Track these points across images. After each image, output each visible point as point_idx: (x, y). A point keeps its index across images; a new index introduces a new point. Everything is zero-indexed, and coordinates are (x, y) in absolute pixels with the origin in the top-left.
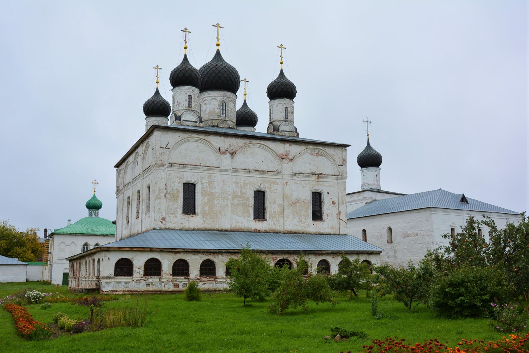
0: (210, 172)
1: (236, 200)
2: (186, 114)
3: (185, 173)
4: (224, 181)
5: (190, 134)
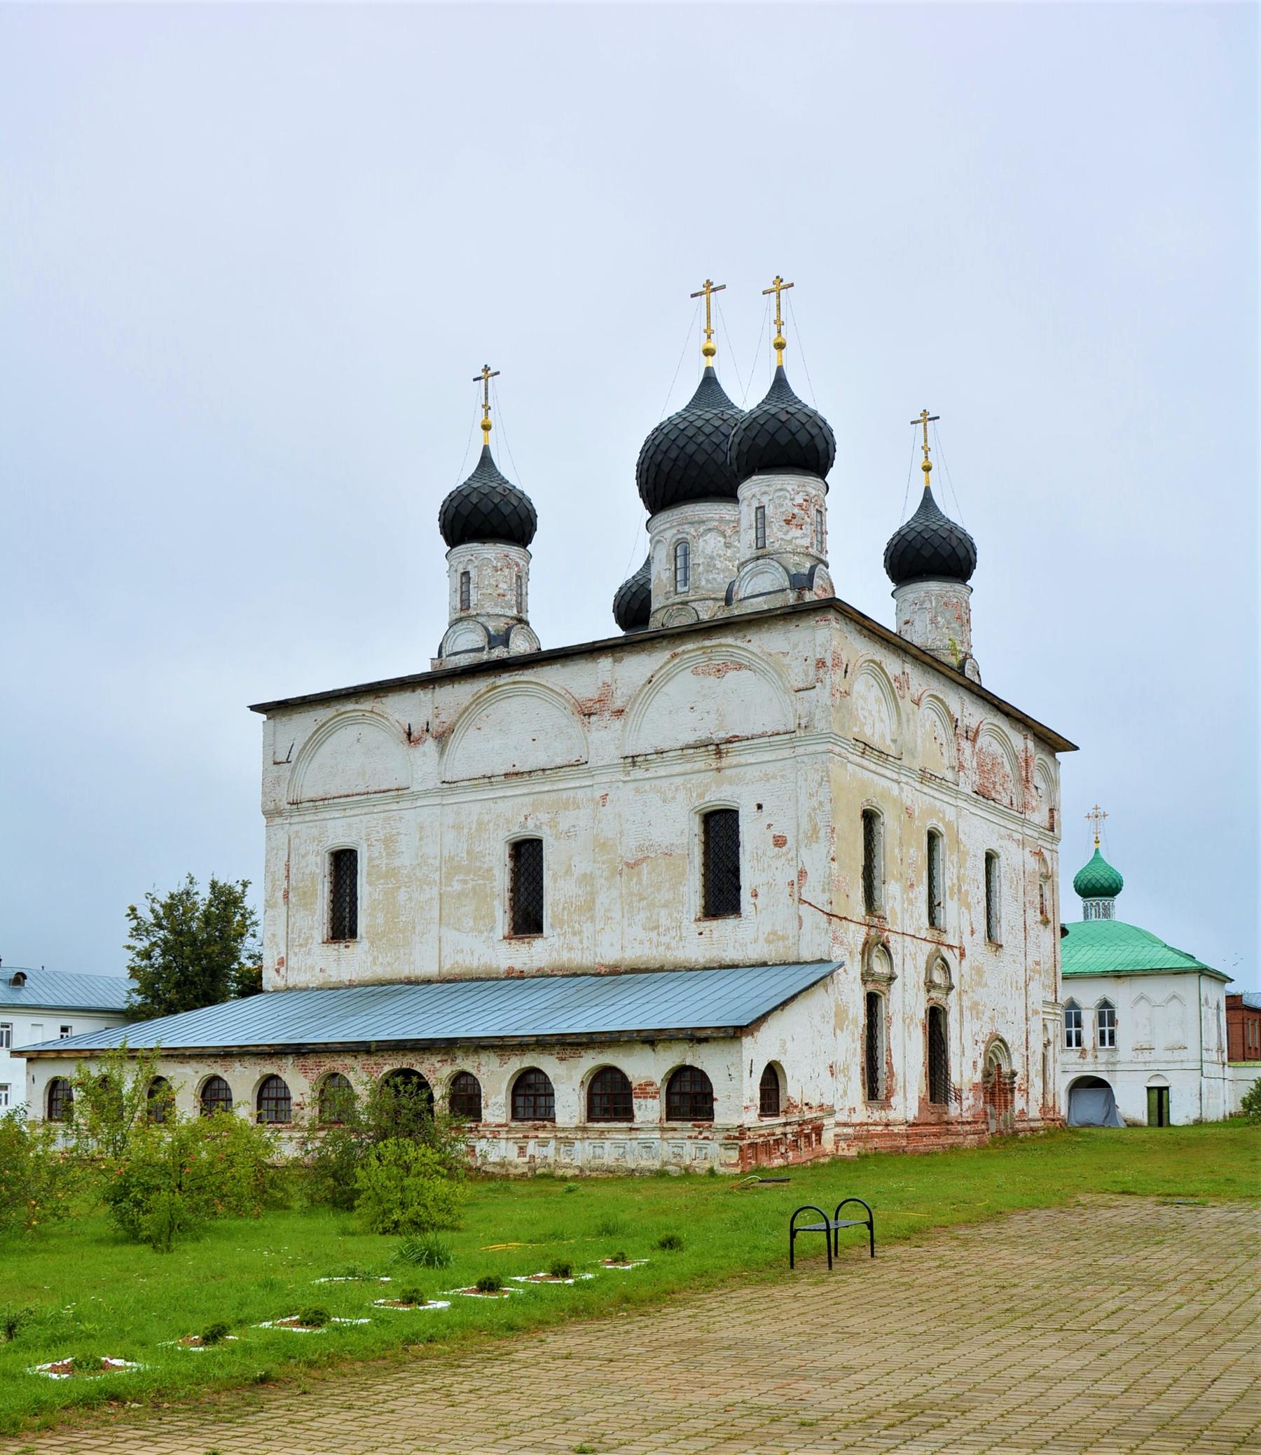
0: (387, 808)
1: (455, 883)
2: (454, 632)
3: (330, 824)
4: (422, 828)
5: (334, 709)
